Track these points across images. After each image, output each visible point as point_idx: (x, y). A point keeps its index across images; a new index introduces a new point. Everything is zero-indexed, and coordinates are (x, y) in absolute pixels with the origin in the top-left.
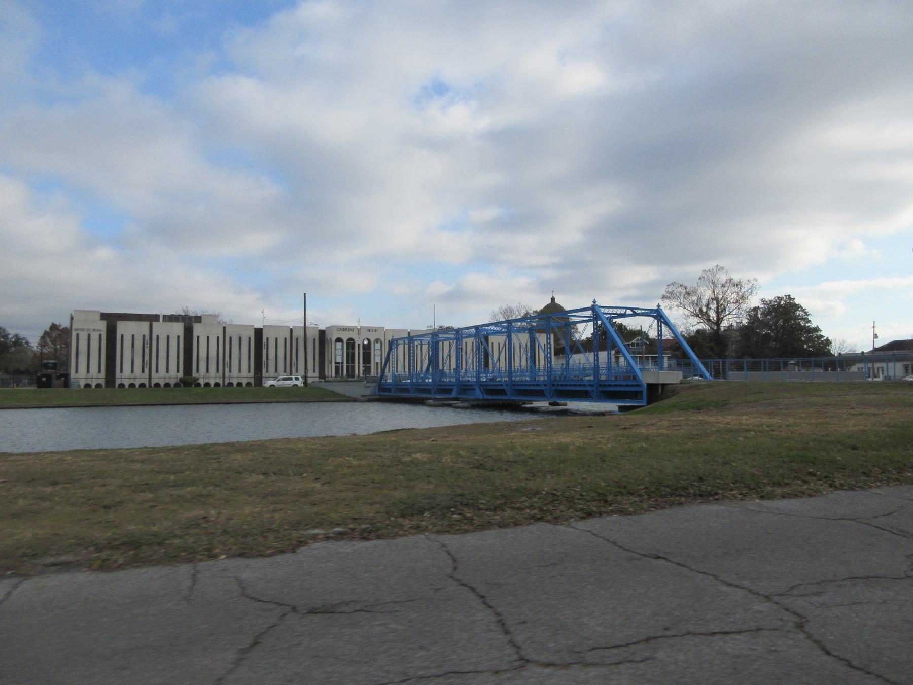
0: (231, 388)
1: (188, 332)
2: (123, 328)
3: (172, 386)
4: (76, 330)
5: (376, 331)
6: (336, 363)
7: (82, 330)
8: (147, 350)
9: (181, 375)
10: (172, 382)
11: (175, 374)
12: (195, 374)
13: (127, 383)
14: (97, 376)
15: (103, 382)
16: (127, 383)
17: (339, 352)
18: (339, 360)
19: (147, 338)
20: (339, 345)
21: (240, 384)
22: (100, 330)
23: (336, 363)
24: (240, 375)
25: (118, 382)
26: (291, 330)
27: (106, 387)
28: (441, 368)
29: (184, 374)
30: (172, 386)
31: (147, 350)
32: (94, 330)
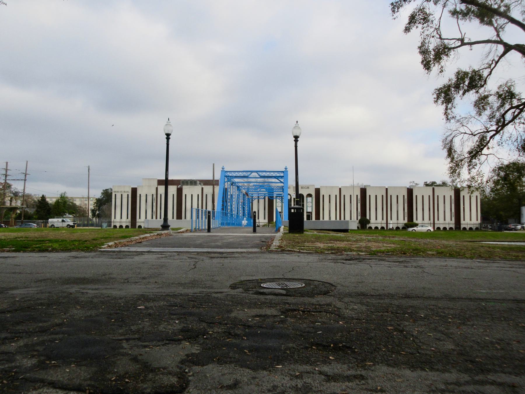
0: (121, 229)
1: (180, 192)
2: (187, 190)
3: (401, 228)
4: (115, 192)
5: (308, 188)
6: (307, 212)
7: (118, 192)
8: (155, 204)
9: (406, 221)
10: (401, 226)
11: (402, 221)
12: (415, 220)
13: (118, 225)
14: (126, 221)
15: (453, 226)
16: (118, 225)
17: (310, 204)
18: (309, 210)
19: (155, 196)
20: (309, 199)
21: (121, 227)
22: (127, 192)
23: (307, 212)
24: (424, 222)
25: (138, 224)
26: (387, 189)
27: (131, 227)
28: (368, 218)
29: (408, 221)
30: (401, 228)
31: (155, 204)
32: (124, 192)
